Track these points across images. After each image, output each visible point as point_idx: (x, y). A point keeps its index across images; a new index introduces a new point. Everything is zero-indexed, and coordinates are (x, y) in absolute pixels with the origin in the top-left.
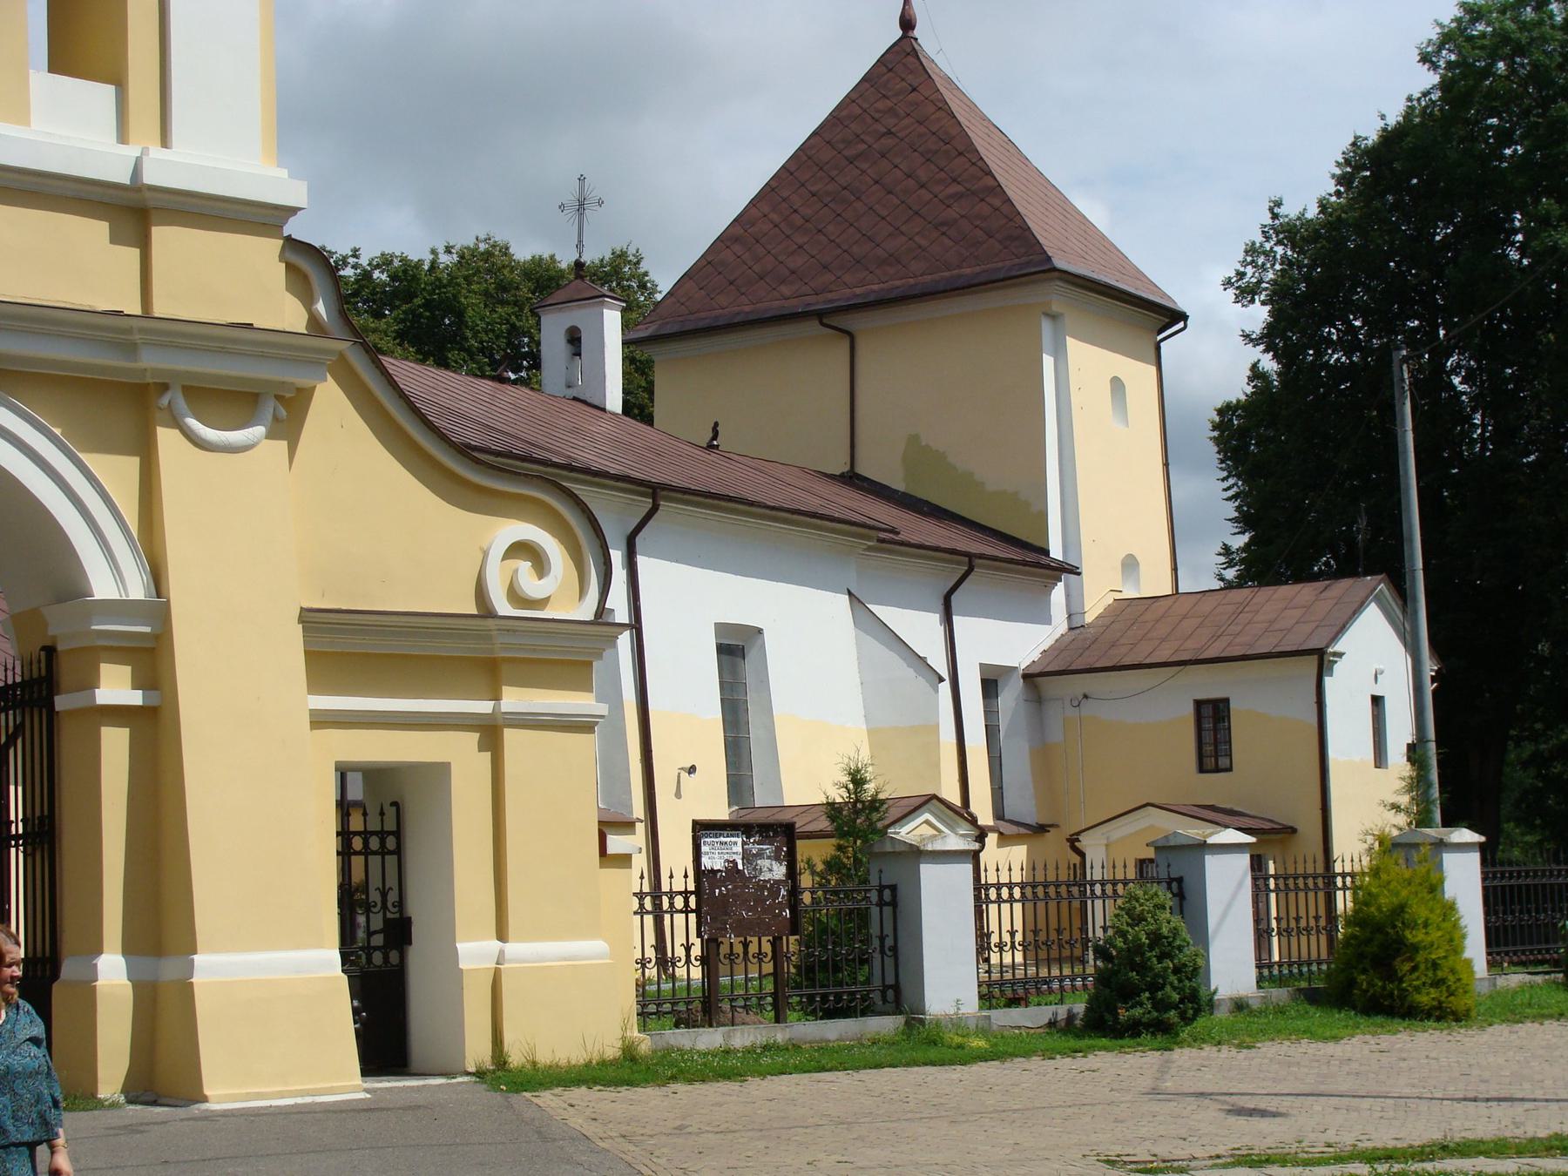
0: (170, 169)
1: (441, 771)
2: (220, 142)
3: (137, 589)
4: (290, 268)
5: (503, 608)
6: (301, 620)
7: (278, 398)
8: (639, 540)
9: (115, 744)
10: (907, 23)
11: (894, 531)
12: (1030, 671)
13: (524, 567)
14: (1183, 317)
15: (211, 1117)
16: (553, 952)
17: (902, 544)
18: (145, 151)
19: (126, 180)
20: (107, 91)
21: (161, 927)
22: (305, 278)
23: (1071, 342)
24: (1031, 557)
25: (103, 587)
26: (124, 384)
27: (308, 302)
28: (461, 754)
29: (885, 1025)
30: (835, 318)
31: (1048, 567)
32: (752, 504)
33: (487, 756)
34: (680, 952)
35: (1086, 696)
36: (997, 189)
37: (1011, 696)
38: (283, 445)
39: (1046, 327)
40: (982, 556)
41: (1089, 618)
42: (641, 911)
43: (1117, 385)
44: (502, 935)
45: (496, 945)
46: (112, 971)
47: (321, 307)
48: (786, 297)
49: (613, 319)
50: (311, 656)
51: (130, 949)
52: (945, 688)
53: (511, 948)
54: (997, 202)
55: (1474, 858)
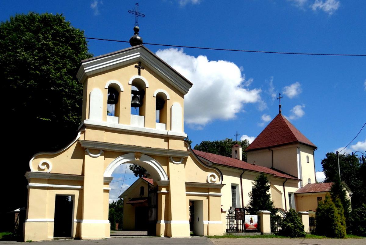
0: (171, 133)
1: (202, 201)
2: (178, 130)
3: (166, 179)
4: (185, 143)
5: (210, 182)
6: (185, 183)
7: (183, 158)
8: (242, 176)
9: (164, 197)
10: (280, 112)
11: (276, 175)
12: (297, 193)
13: (212, 178)
14: (317, 148)
15: (172, 239)
16: (216, 224)
17: (277, 176)
18: (168, 131)
19: (166, 134)
20: (165, 124)
21: (168, 218)
22: (187, 144)
23: (301, 152)
24: (295, 178)
25: (163, 179)
26: (166, 158)
27: (187, 148)
28: (204, 199)
29: (259, 234)
30: (270, 148)
31: (298, 180)
32: (257, 171)
33: (207, 200)
34: (239, 223)
35: (303, 196)
36: (291, 132)
37: (292, 197)
38: (183, 165)
39: (298, 149)
40: (289, 178)
41: (303, 186)
42: (227, 218)
43: (307, 157)
44: (209, 220)
45: (208, 221)
46: (163, 223)
47: (188, 148)
48: (264, 146)
49: (241, 149)
50: (186, 187)
51: (165, 220)
52: (283, 195)
53: (210, 222)
54: (291, 134)
55: (269, 216)
